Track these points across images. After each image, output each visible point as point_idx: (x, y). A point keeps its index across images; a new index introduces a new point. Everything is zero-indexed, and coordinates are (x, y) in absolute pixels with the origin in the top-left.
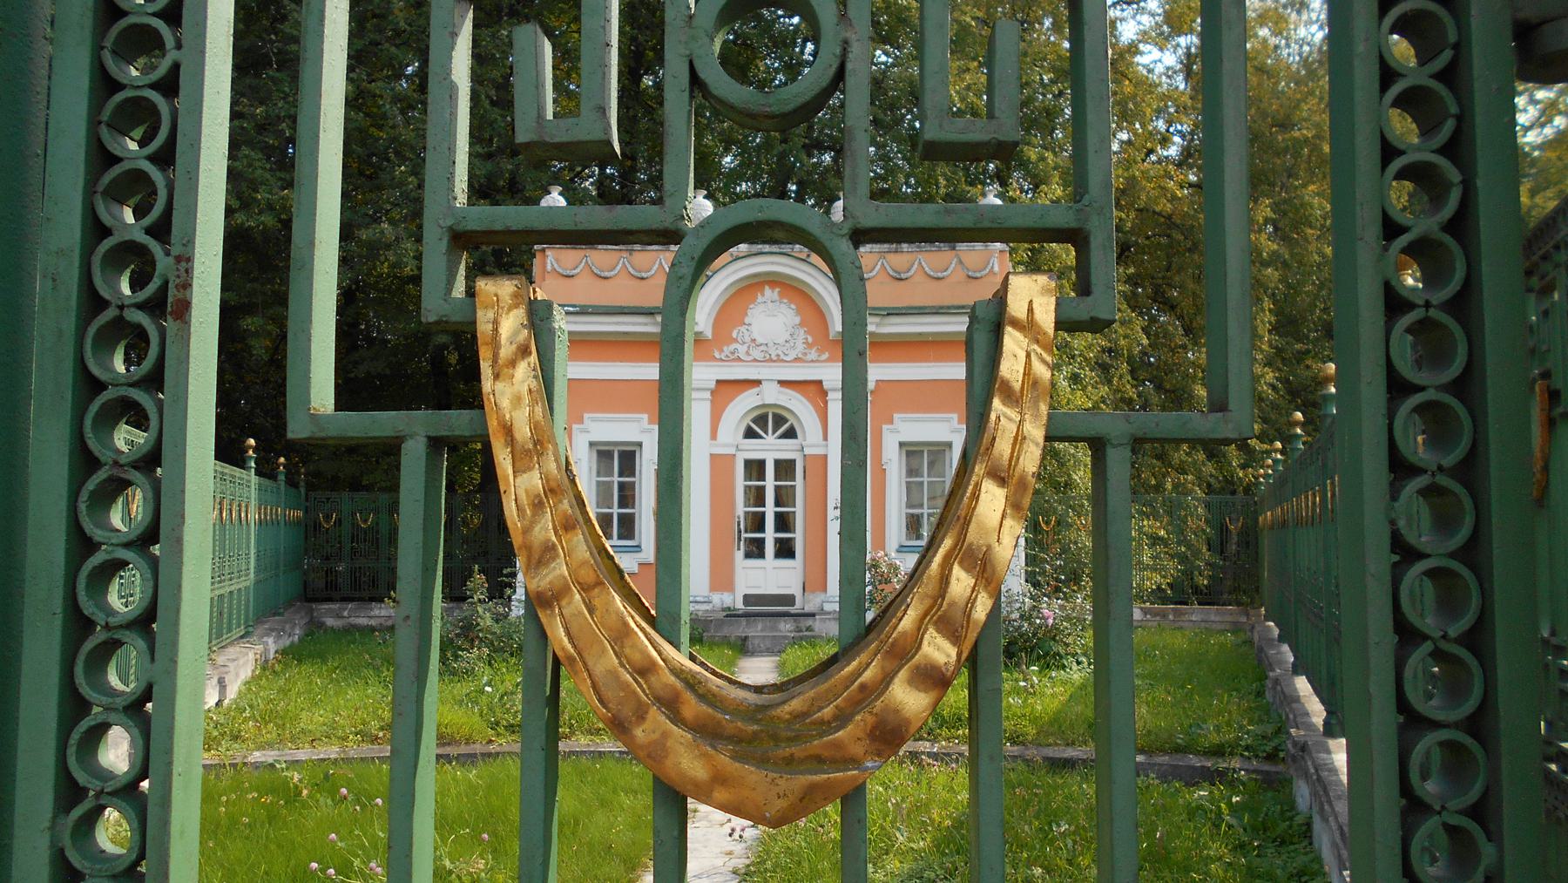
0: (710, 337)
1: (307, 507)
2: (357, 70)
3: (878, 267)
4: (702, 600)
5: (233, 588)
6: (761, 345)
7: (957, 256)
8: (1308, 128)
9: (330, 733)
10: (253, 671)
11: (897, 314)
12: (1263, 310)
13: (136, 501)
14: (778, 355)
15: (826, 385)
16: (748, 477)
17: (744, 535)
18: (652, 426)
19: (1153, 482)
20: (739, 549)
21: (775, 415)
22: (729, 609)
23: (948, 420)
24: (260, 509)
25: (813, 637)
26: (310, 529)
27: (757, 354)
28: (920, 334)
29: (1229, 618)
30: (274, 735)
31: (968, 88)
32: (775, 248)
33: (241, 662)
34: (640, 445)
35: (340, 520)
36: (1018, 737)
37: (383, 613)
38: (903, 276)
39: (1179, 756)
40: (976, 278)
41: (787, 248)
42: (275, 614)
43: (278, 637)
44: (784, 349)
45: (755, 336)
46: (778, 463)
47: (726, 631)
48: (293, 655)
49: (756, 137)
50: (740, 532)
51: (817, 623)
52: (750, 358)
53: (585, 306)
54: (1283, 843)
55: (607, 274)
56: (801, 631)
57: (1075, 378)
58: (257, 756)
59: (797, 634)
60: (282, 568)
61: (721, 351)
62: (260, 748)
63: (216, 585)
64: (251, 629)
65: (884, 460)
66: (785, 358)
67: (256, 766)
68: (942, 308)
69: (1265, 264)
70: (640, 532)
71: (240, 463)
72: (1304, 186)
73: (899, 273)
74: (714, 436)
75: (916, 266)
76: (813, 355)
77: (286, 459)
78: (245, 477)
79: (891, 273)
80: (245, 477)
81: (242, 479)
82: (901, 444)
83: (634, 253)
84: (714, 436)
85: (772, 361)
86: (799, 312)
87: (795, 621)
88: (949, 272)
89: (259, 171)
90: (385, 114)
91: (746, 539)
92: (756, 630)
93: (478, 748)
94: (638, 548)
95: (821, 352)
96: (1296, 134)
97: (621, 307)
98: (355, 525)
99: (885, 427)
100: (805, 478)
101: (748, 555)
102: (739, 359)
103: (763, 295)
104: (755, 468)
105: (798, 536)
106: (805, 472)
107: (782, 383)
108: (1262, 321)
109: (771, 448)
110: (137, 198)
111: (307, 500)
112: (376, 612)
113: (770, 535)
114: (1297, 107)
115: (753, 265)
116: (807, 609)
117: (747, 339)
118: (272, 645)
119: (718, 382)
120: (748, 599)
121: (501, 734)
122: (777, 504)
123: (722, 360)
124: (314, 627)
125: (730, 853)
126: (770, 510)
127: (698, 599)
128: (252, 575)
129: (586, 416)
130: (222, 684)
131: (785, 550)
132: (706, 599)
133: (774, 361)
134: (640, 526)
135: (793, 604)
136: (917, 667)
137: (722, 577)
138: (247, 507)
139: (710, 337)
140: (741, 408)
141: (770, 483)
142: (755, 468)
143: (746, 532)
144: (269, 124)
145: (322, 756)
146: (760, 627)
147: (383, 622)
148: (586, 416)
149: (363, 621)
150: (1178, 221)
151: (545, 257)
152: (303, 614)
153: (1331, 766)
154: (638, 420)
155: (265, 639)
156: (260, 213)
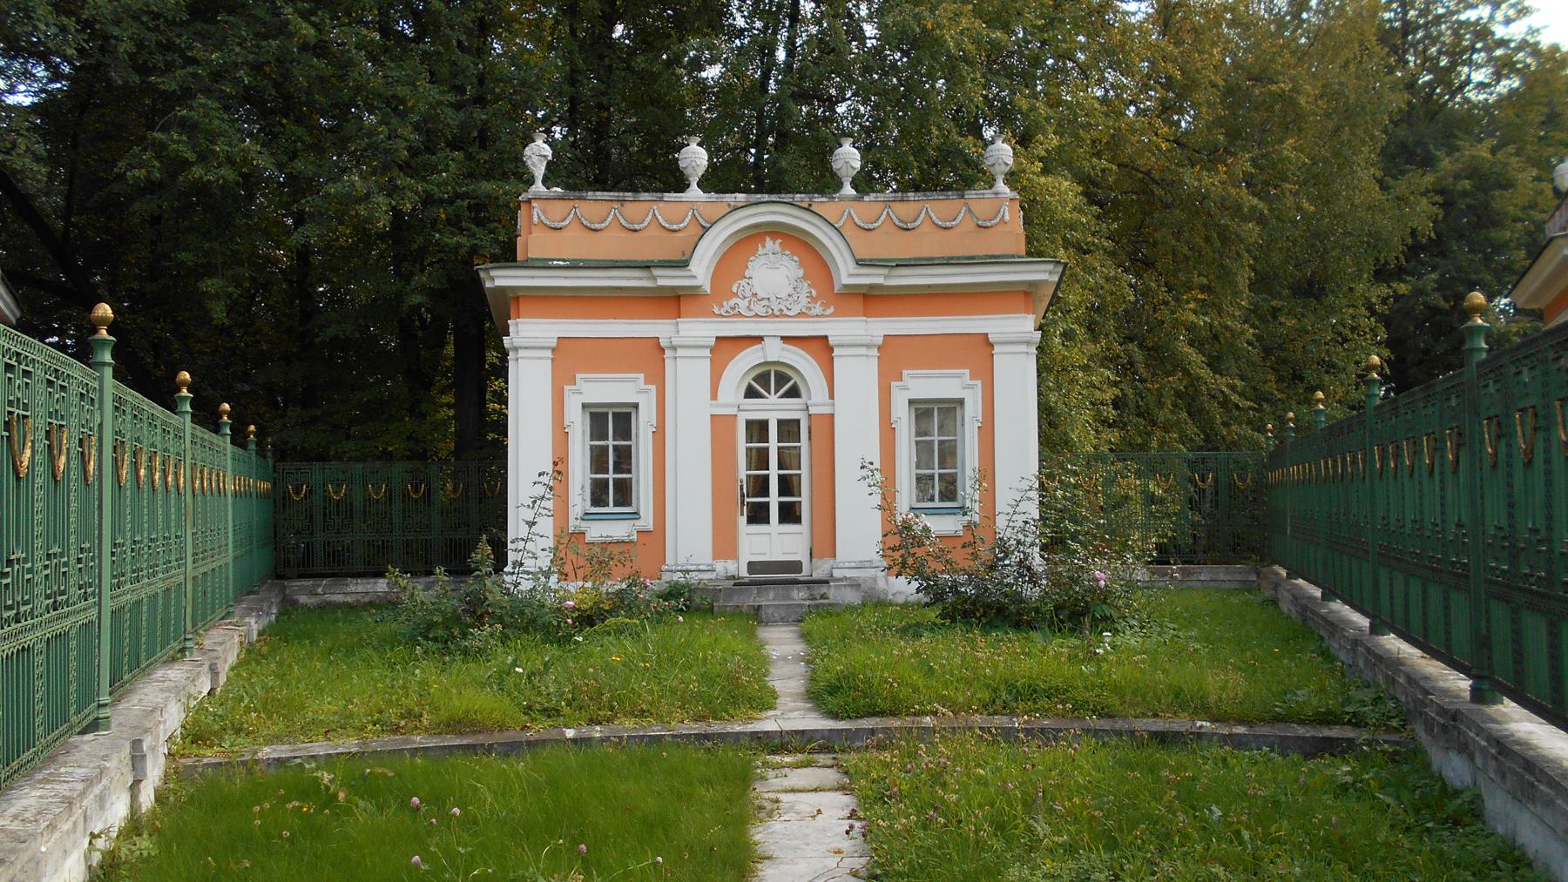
0: (709, 292)
1: (275, 479)
2: (320, 13)
3: (884, 217)
4: (705, 568)
5: (214, 565)
6: (763, 299)
7: (966, 204)
8: (1284, 82)
9: (343, 724)
10: (238, 656)
11: (906, 265)
12: (1243, 266)
13: (125, 466)
14: (781, 310)
15: (831, 341)
16: (750, 439)
17: (747, 500)
18: (650, 387)
19: (1140, 441)
20: (742, 514)
22: (734, 576)
23: (959, 376)
24: (235, 479)
25: (830, 605)
26: (278, 501)
27: (758, 309)
28: (929, 286)
29: (1238, 577)
30: (281, 725)
31: (962, 33)
32: (774, 198)
33: (229, 644)
34: (636, 406)
35: (311, 492)
36: (1103, 709)
37: (360, 589)
38: (910, 226)
39: (1282, 725)
40: (987, 227)
41: (787, 198)
42: (249, 593)
43: (259, 617)
44: (787, 303)
46: (780, 423)
47: (736, 601)
48: (278, 634)
50: (742, 496)
51: (832, 590)
53: (575, 260)
54: (1456, 823)
55: (597, 226)
56: (815, 599)
57: (1068, 335)
58: (267, 752)
59: (813, 602)
60: (255, 543)
62: (268, 742)
63: (200, 562)
64: (231, 609)
65: (894, 418)
67: (269, 763)
68: (952, 258)
69: (1245, 219)
70: (638, 499)
71: (216, 429)
72: (1281, 141)
73: (906, 223)
74: (714, 396)
75: (923, 215)
76: (818, 309)
77: (1301, 13)
78: (222, 443)
79: (897, 223)
80: (222, 443)
81: (219, 446)
82: (911, 402)
83: (626, 204)
84: (714, 396)
86: (801, 264)
87: (809, 588)
88: (958, 220)
89: (216, 122)
90: (350, 59)
91: (748, 503)
92: (769, 599)
93: (510, 736)
95: (826, 306)
96: (1274, 88)
97: (612, 261)
98: (327, 499)
99: (894, 384)
100: (810, 439)
102: (740, 315)
103: (764, 246)
104: (758, 429)
105: (804, 499)
106: (810, 432)
107: (785, 339)
108: (1243, 277)
109: (773, 408)
111: (275, 471)
112: (352, 588)
113: (774, 499)
114: (1272, 60)
115: (755, 215)
116: (816, 576)
117: (748, 294)
118: (254, 625)
119: (717, 338)
120: (752, 567)
121: (536, 720)
122: (780, 468)
124: (288, 606)
125: (839, 852)
126: (774, 473)
127: (701, 567)
128: (230, 552)
130: (214, 672)
131: (790, 514)
132: (709, 568)
133: (777, 316)
134: (638, 492)
135: (800, 571)
137: (725, 544)
138: (224, 476)
139: (709, 292)
140: (744, 364)
141: (773, 444)
143: (748, 496)
144: (225, 72)
145: (340, 750)
146: (771, 596)
147: (360, 598)
149: (339, 598)
150: (1157, 177)
151: (531, 208)
153: (1511, 739)
154: (634, 380)
155: (247, 620)
156: (220, 165)
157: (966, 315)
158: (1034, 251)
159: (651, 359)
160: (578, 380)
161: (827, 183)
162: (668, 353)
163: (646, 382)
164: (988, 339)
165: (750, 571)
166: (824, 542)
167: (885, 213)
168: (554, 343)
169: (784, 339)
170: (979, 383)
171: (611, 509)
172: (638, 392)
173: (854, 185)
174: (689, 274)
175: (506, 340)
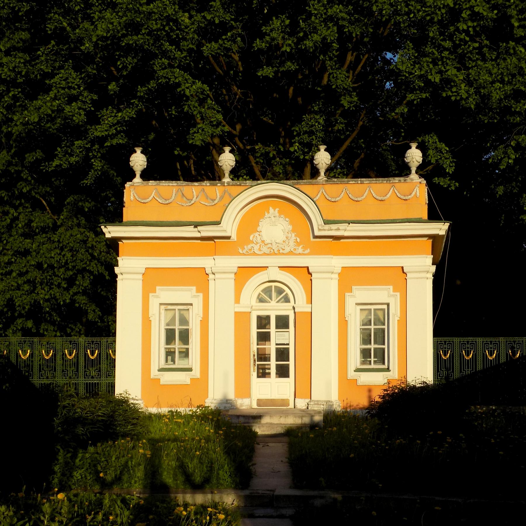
17: (257, 363)
27: (265, 250)
35: (32, 354)
45: (265, 238)
50: (255, 361)
52: (262, 252)
65: (150, 315)
66: (284, 252)
74: (237, 300)
76: (300, 250)
84: (237, 300)
85: (276, 254)
86: (291, 223)
95: (304, 248)
99: (151, 295)
100: (295, 327)
101: (258, 377)
110: (214, 152)
113: (273, 363)
123: (244, 254)
129: (158, 288)
131: (283, 372)
136: (134, 176)
142: (264, 322)
148: (158, 288)
152: (147, 413)
157: (176, 256)
160: (354, 290)
162: (211, 276)
163: (394, 291)
164: (403, 270)
165: (258, 405)
167: (391, 190)
168: (235, 269)
169: (279, 267)
170: (398, 294)
172: (192, 297)
174: (221, 229)
175: (116, 269)
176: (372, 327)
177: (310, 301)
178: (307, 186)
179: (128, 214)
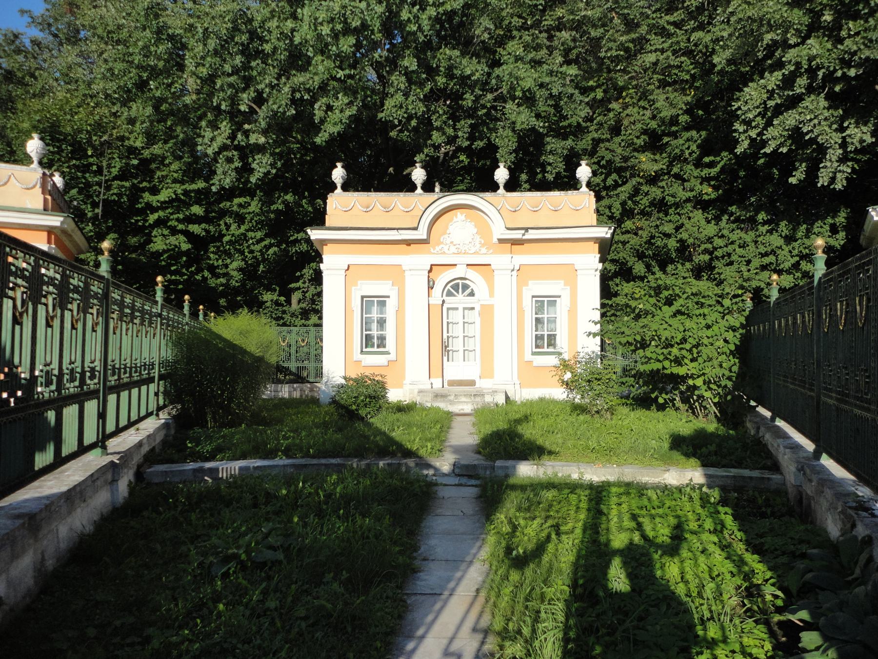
21: (472, 290)
49: (254, 594)
61: (434, 249)
83: (479, 637)
94: (388, 353)
99: (524, 288)
102: (444, 253)
129: (530, 282)
136: (336, 188)
158: (600, 223)
159: (396, 274)
161: (494, 187)
166: (487, 371)
171: (375, 349)
173: (422, 188)
176: (545, 316)
177: (492, 294)
178: (488, 195)
179: (329, 221)
